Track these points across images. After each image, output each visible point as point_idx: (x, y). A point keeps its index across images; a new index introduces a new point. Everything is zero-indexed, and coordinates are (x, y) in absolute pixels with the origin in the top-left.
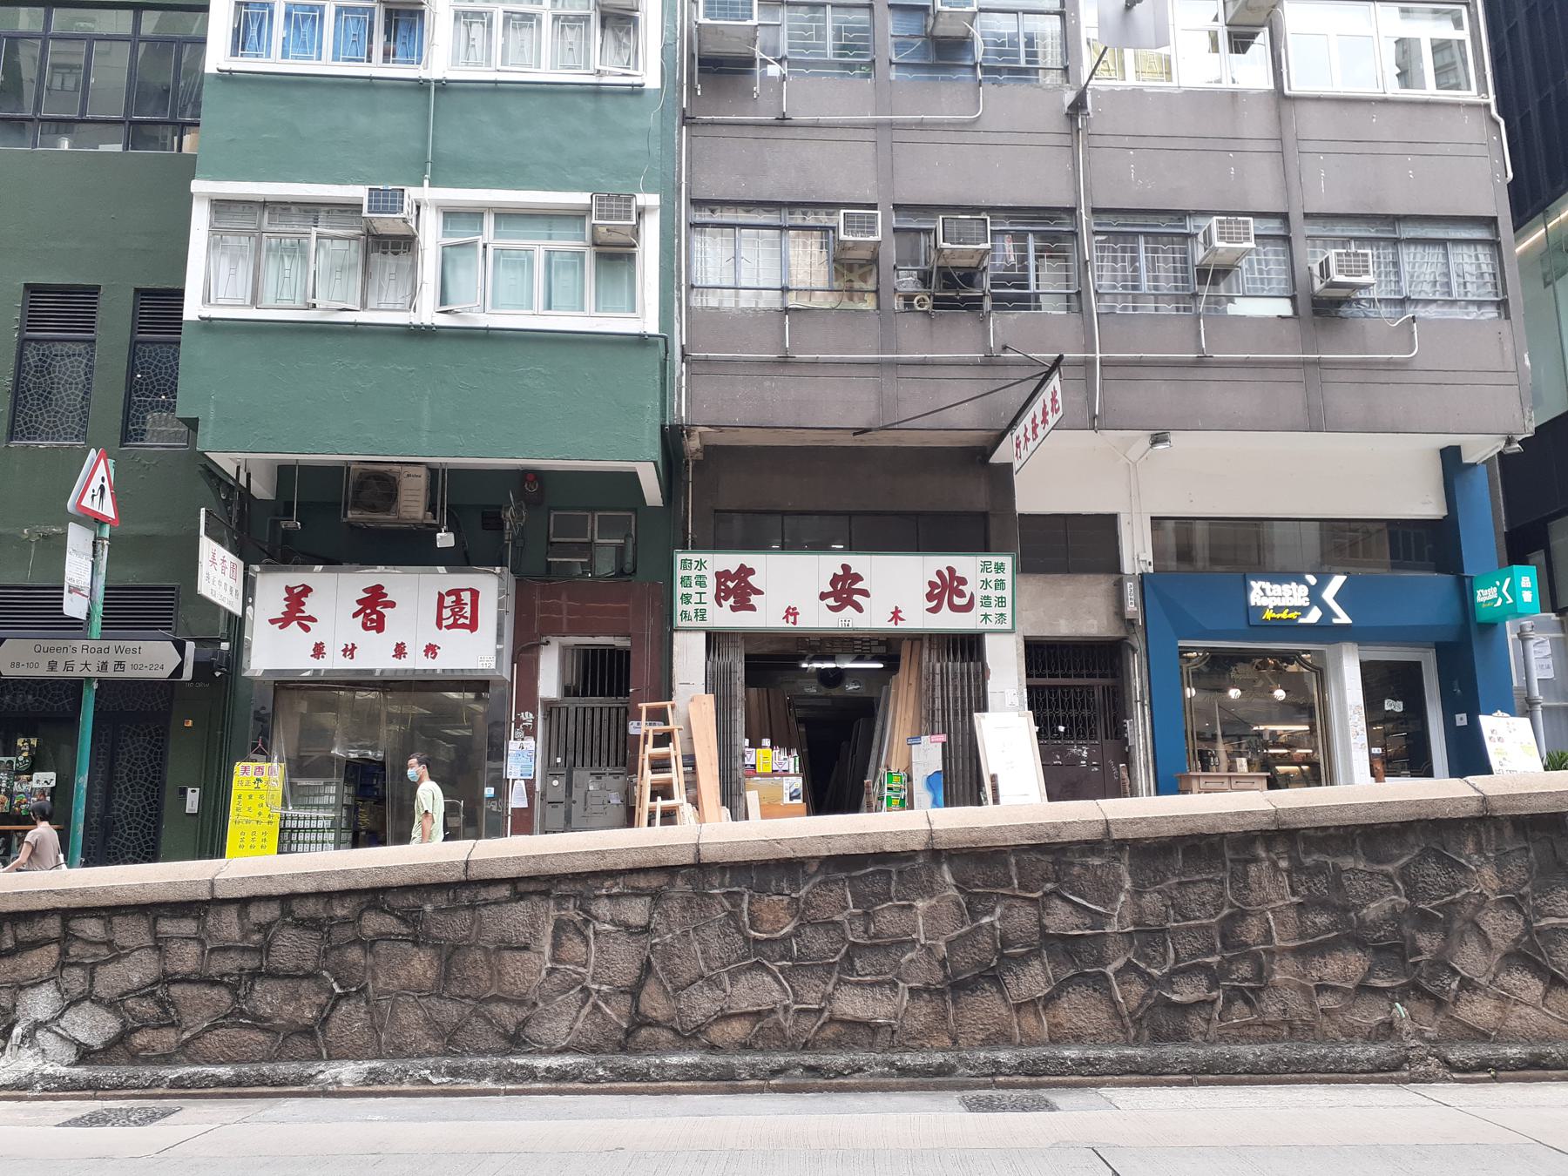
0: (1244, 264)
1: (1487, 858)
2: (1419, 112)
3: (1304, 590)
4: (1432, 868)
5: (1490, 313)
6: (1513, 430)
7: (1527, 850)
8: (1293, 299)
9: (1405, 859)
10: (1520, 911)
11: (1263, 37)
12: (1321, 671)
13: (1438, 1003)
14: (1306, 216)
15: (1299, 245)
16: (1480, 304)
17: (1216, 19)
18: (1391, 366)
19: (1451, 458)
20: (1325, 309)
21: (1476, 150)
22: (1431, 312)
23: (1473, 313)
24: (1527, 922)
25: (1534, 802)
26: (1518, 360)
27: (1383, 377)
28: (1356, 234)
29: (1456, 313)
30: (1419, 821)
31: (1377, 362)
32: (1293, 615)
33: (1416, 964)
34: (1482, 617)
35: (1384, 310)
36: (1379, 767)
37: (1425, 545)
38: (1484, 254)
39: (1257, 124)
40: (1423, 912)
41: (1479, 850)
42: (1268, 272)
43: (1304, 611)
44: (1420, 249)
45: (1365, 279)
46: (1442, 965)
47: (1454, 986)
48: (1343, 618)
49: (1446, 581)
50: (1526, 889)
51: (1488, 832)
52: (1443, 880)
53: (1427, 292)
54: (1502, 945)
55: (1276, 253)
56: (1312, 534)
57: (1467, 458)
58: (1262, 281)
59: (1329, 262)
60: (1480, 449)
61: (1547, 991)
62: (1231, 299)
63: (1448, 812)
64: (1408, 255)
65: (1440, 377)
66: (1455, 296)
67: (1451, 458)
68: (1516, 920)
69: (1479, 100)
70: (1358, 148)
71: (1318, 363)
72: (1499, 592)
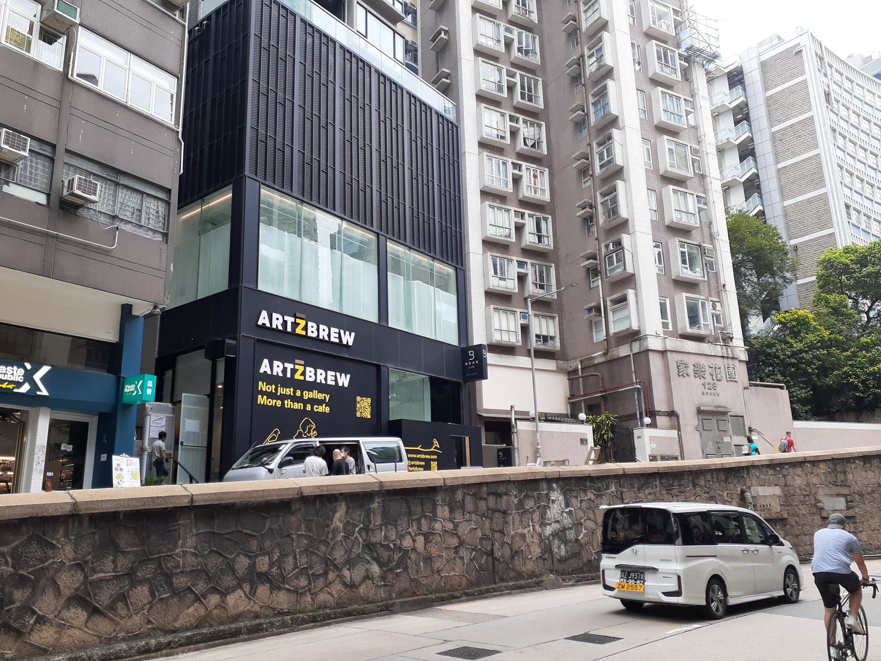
0: (20, 164)
1: (70, 540)
2: (143, 120)
3: (21, 371)
4: (34, 547)
5: (159, 238)
6: (157, 301)
7: (94, 533)
8: (48, 196)
9: (16, 543)
10: (83, 570)
11: (63, 40)
12: (24, 423)
13: (19, 634)
14: (67, 151)
15: (58, 165)
16: (155, 232)
17: (35, 16)
18: (99, 251)
19: (126, 310)
20: (67, 208)
21: (168, 152)
22: (128, 228)
23: (150, 235)
24: (86, 577)
25: (104, 505)
26: (168, 267)
27: (94, 255)
28: (95, 172)
29: (141, 233)
30: (31, 518)
31: (91, 246)
32: (10, 387)
33: (9, 610)
34: (126, 400)
35: (102, 219)
36: (49, 484)
37: (105, 356)
38: (161, 208)
39: (48, 88)
40: (22, 577)
41: (66, 535)
42: (36, 175)
43: (19, 384)
44: (129, 193)
45: (92, 197)
46: (27, 609)
47: (32, 622)
48: (44, 392)
49: (111, 377)
50: (89, 557)
51: (74, 524)
52: (39, 554)
53: (127, 216)
54: (67, 592)
55: (44, 165)
56: (67, 344)
57: (135, 312)
58: (31, 179)
59: (73, 181)
60: (141, 309)
61: (89, 617)
62: (7, 183)
63: (52, 512)
64: (122, 194)
65: (126, 264)
66: (142, 223)
67: (126, 310)
68: (80, 576)
69: (173, 127)
70: (105, 125)
71: (56, 237)
72: (136, 388)
